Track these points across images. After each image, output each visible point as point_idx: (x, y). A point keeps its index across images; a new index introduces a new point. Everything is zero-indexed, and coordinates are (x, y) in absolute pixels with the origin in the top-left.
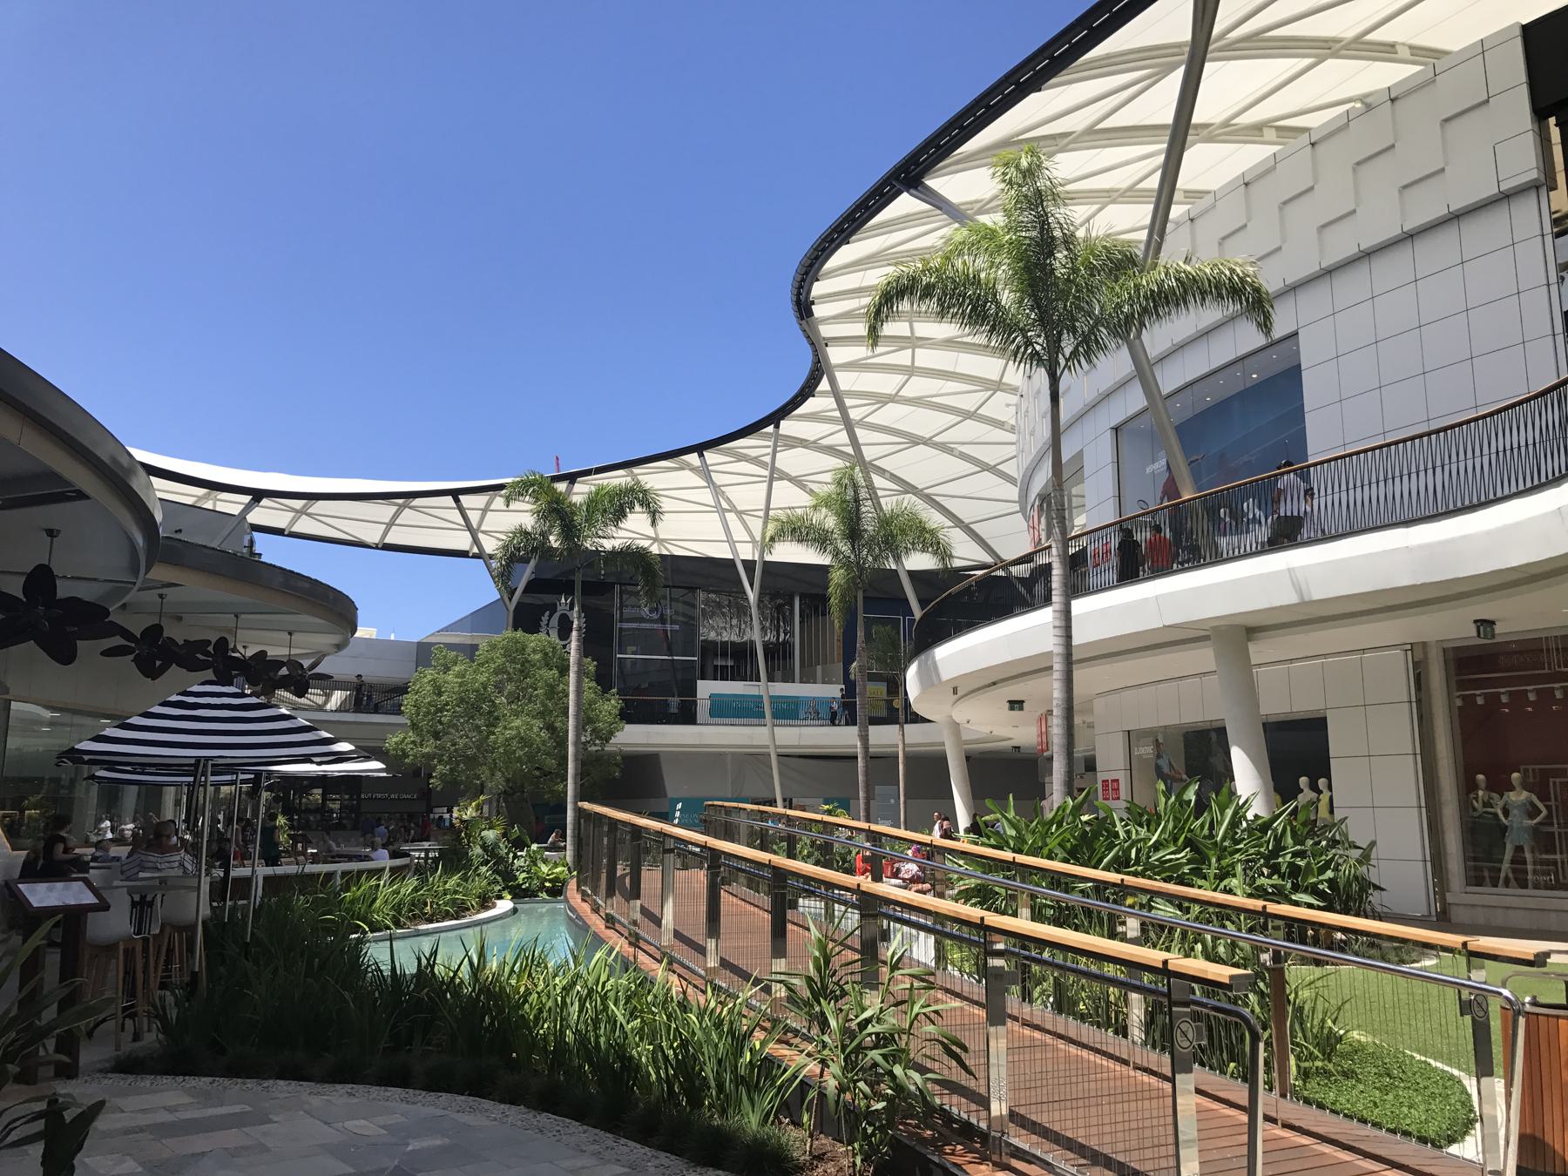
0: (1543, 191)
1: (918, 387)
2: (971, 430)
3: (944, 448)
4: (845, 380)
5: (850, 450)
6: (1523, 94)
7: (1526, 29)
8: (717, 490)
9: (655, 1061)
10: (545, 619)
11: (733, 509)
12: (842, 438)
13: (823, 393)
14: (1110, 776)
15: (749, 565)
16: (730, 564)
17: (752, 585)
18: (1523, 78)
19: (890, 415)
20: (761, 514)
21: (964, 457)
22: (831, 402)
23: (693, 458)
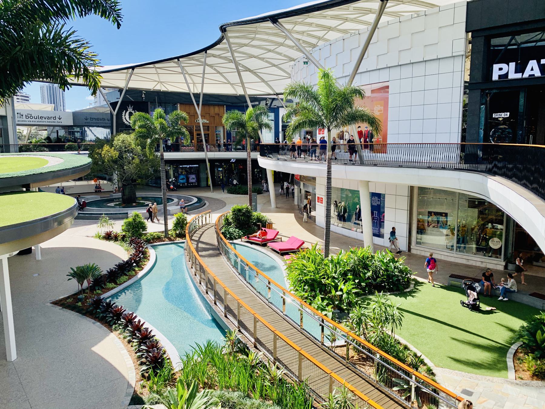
0: (464, 57)
1: (255, 43)
2: (270, 55)
3: (262, 59)
4: (231, 40)
5: (231, 58)
6: (464, 25)
7: (468, 3)
8: (183, 68)
9: (268, 362)
10: (124, 113)
11: (187, 73)
12: (229, 54)
13: (225, 43)
14: (320, 196)
15: (197, 96)
16: (188, 94)
17: (198, 105)
18: (465, 20)
19: (244, 49)
20: (201, 75)
21: (267, 62)
22: (227, 46)
23: (176, 60)
